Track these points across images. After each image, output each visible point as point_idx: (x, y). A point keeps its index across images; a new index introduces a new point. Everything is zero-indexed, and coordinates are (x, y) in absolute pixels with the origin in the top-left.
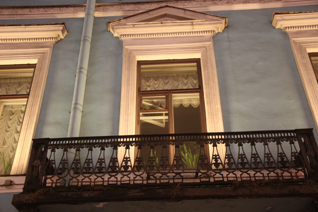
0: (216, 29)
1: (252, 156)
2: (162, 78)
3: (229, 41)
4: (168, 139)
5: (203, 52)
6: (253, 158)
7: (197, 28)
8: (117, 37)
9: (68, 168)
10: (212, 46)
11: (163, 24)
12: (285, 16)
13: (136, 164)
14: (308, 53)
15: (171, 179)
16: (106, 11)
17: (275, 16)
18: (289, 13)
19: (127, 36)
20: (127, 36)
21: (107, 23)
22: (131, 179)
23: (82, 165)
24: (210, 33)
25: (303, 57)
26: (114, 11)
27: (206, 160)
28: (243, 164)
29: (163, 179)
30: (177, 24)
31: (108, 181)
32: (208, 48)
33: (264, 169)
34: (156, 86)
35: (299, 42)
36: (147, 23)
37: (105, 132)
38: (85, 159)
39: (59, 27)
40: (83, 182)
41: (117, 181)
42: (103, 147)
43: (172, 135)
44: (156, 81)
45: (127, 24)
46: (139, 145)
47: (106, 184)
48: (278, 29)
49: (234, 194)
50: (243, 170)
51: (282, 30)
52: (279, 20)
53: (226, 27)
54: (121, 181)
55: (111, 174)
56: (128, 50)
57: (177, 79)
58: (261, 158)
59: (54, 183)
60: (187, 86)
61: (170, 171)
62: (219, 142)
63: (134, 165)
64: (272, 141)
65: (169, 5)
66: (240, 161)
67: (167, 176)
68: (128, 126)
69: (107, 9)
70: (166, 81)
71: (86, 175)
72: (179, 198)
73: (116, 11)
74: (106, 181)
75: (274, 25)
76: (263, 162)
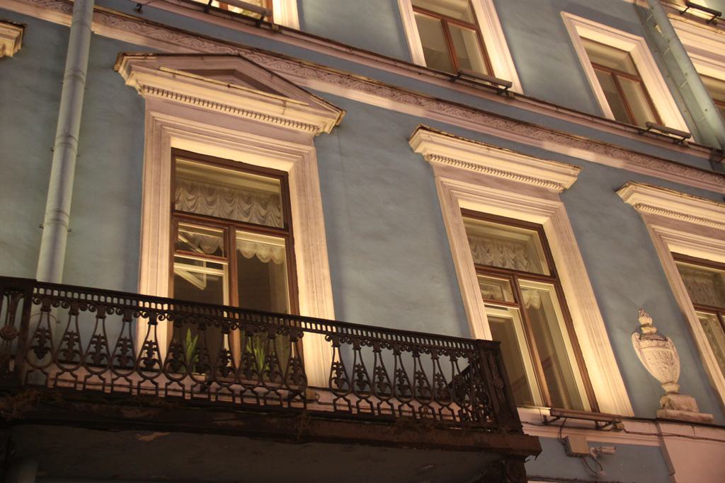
0: (321, 126)
1: (374, 371)
2: (201, 190)
3: (341, 154)
4: (276, 323)
5: (297, 162)
6: (93, 344)
7: (291, 115)
8: (133, 88)
9: (109, 354)
10: (313, 155)
11: (231, 90)
12: (434, 136)
13: (171, 357)
14: (172, 148)
15: (237, 396)
16: (112, 27)
17: (420, 131)
18: (440, 133)
19: (155, 92)
20: (155, 92)
21: (119, 54)
22: (79, 379)
23: (112, 349)
24: (312, 129)
25: (454, 213)
26: (129, 31)
27: (182, 355)
28: (361, 383)
29: (272, 399)
30: (256, 96)
31: (166, 390)
32: (306, 157)
33: (351, 392)
34: (191, 204)
35: (450, 186)
36: (202, 78)
37: (110, 280)
38: (64, 332)
39: (11, 31)
40: (170, 390)
41: (104, 385)
42: (102, 310)
43: (226, 308)
44: (190, 192)
45: (161, 69)
46: (172, 316)
47: (80, 387)
48: (417, 154)
49: (396, 440)
50: (382, 397)
51: (423, 157)
52: (425, 140)
53: (336, 127)
54: (84, 383)
55: (144, 373)
56: (156, 121)
57: (231, 199)
58: (348, 373)
59: (51, 379)
60: (249, 218)
61: (259, 383)
62: (112, 311)
63: (166, 358)
64: (117, 313)
65: (242, 53)
66: (64, 346)
67: (278, 394)
68: (155, 281)
69: (113, 23)
70: (210, 199)
71: (66, 366)
72: (307, 438)
73: (132, 32)
74: (162, 389)
75: (412, 146)
76: (351, 380)
